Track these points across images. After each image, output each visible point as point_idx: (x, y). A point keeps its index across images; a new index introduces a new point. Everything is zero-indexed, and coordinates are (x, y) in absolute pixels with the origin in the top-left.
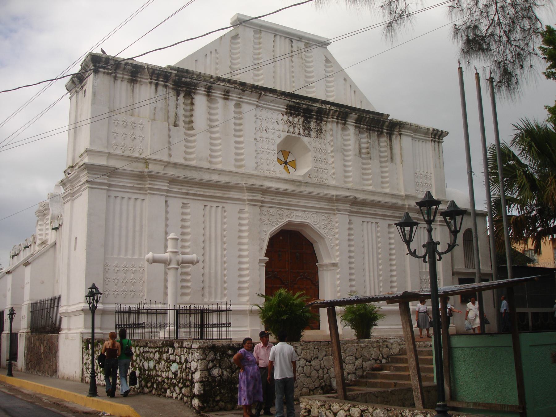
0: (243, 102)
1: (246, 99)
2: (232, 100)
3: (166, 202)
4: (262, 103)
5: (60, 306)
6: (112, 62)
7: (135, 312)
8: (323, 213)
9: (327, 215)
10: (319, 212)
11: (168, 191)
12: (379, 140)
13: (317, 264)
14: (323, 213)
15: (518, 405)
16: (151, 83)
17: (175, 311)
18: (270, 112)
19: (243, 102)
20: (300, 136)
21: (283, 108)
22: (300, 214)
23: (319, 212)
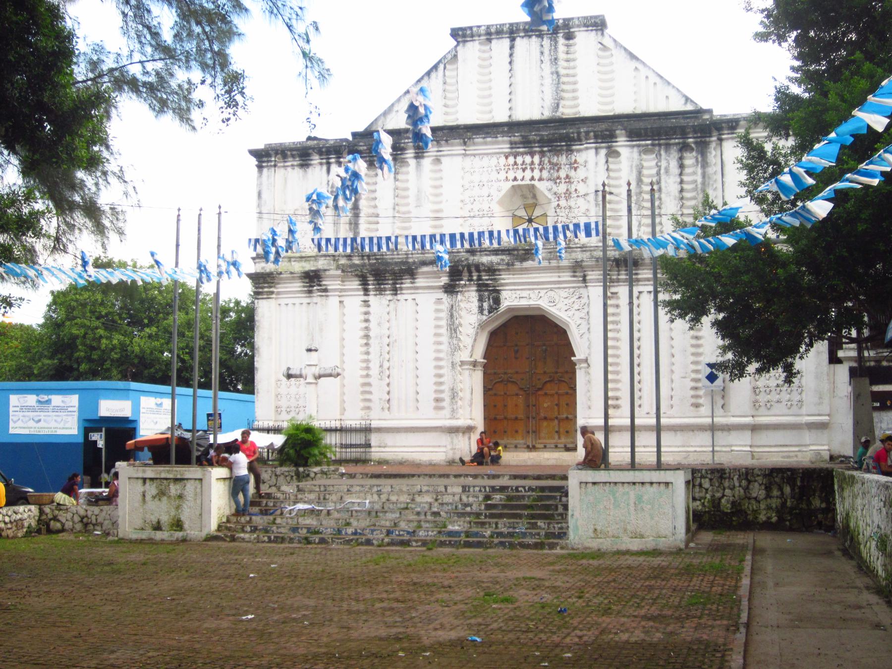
0: (443, 156)
1: (446, 149)
2: (429, 156)
3: (341, 302)
4: (472, 149)
5: (811, 200)
6: (564, 525)
7: (657, 195)
8: (565, 288)
9: (572, 290)
10: (559, 288)
11: (341, 290)
12: (681, 158)
13: (573, 358)
14: (565, 288)
15: (20, 181)
16: (321, 164)
17: (610, 159)
18: (486, 158)
19: (443, 156)
20: (533, 182)
21: (506, 148)
22: (525, 294)
23: (559, 288)
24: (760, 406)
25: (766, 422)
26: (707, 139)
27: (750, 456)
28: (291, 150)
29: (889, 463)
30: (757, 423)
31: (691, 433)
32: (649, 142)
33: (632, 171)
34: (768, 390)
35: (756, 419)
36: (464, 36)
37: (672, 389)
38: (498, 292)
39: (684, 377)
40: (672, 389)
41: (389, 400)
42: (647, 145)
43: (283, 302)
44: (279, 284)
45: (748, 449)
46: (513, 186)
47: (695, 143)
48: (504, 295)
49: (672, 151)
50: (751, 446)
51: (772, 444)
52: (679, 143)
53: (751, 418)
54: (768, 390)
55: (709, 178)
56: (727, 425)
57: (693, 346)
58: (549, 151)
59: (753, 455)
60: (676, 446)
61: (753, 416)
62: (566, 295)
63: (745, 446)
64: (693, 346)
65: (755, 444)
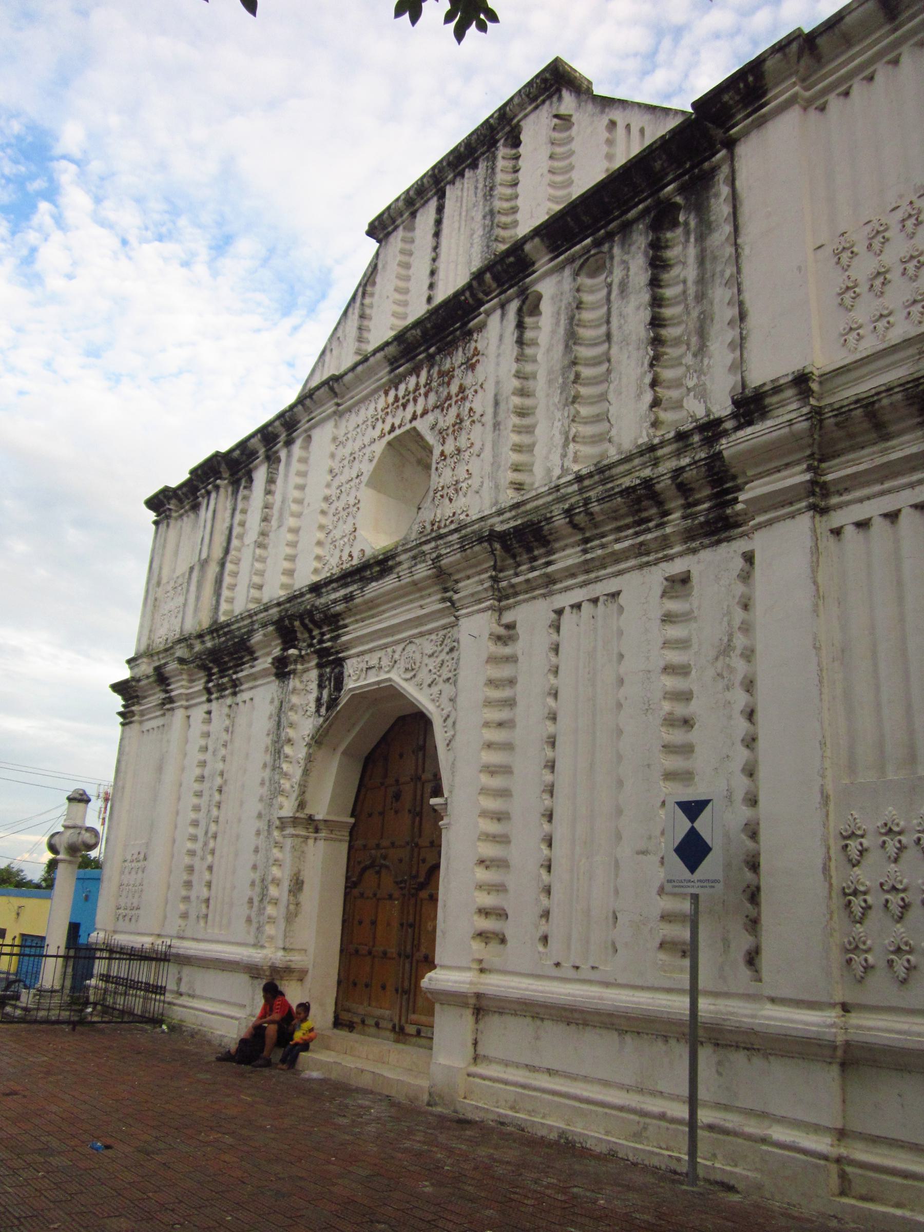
10: (421, 635)
24: (868, 968)
25: (885, 1038)
26: (706, 165)
27: (834, 1181)
28: (501, 680)
29: (922, 811)
30: (855, 1036)
31: (660, 1046)
32: (588, 241)
33: (557, 323)
34: (895, 900)
35: (855, 1019)
36: (384, 227)
37: (617, 892)
38: (340, 662)
39: (644, 852)
40: (617, 892)
41: (207, 901)
42: (587, 250)
43: (148, 725)
44: (145, 697)
45: (822, 1144)
46: (389, 444)
47: (681, 190)
48: (351, 667)
49: (635, 236)
50: (842, 1134)
51: (233, 940)
52: (646, 211)
53: (831, 1016)
54: (895, 900)
55: (715, 258)
56: (752, 1032)
57: (669, 748)
58: (439, 351)
59: (843, 1176)
60: (622, 1087)
61: (846, 1008)
62: (429, 648)
63: (816, 1128)
64: (669, 748)
65: (856, 1126)
